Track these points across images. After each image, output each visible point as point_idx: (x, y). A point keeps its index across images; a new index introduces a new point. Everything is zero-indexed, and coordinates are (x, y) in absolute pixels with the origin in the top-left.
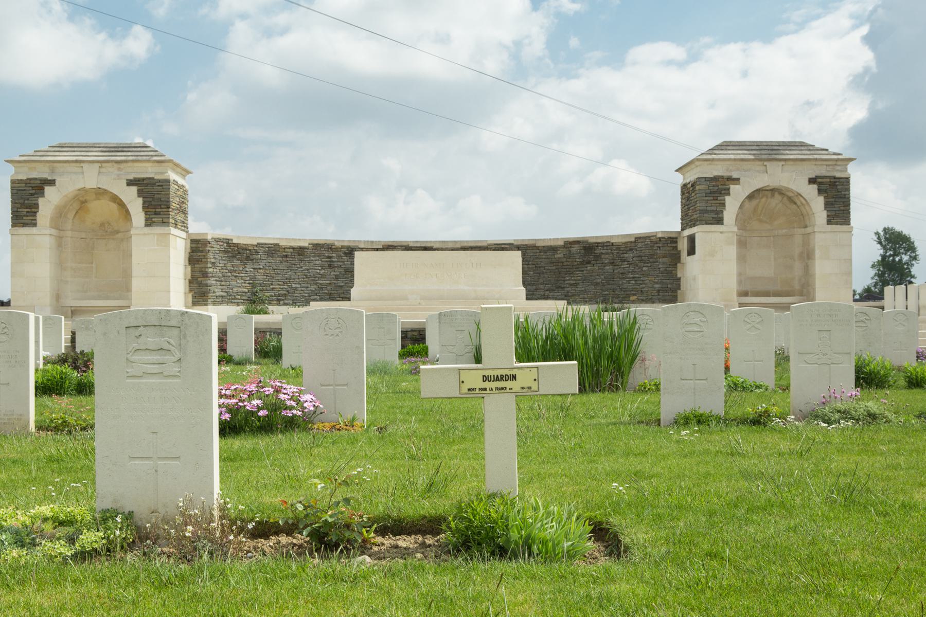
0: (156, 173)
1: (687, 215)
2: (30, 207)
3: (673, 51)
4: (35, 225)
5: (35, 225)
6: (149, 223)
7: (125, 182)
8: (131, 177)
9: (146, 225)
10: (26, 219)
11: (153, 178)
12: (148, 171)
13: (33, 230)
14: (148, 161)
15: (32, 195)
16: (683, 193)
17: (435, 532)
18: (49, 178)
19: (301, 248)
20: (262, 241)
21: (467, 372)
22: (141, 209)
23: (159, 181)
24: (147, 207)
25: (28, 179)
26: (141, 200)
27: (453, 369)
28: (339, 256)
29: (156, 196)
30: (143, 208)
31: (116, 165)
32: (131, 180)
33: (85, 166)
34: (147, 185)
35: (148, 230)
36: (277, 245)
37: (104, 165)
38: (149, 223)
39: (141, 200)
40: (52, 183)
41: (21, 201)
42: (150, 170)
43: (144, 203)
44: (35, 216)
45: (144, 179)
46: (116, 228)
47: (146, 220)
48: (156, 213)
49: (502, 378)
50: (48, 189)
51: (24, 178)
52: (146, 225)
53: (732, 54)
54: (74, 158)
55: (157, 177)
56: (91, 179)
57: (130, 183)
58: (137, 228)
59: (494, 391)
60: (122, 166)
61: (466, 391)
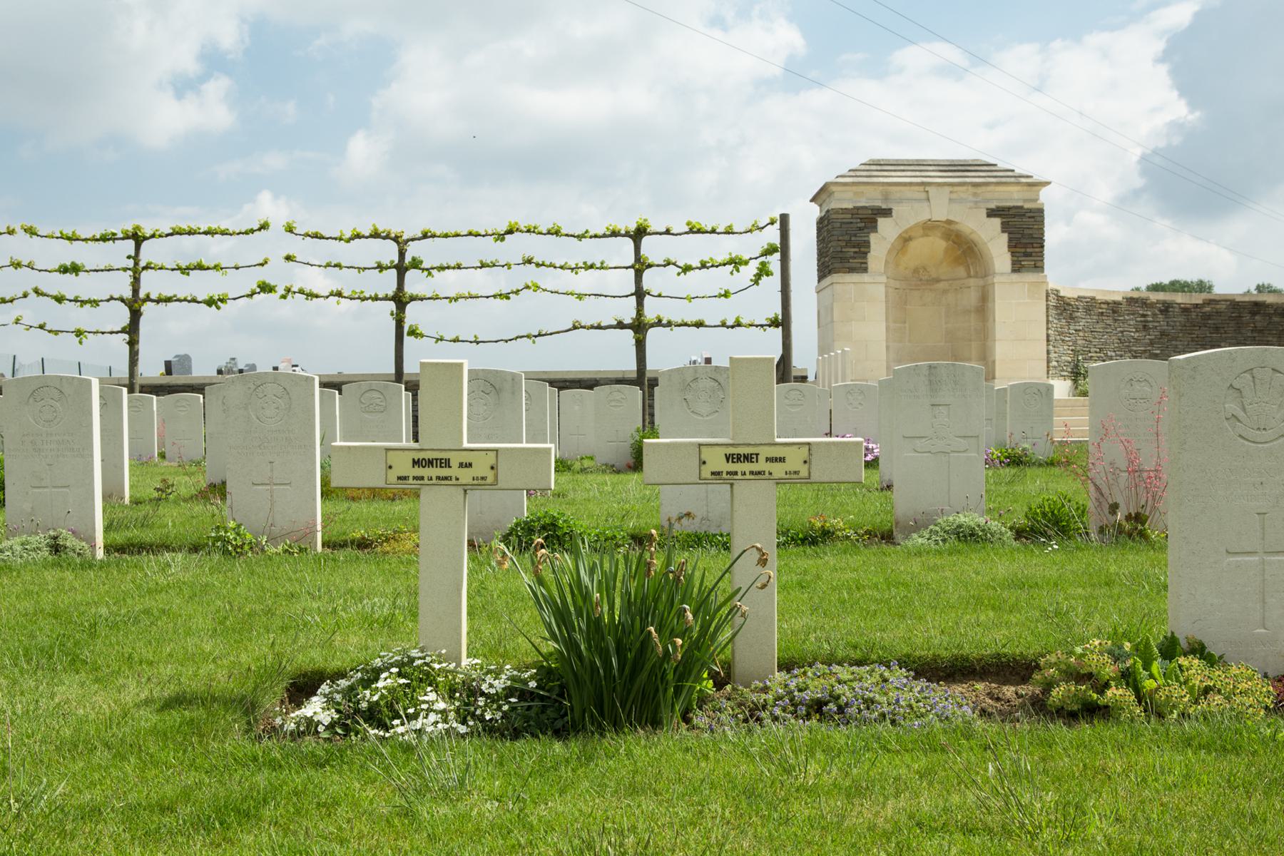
0: (1025, 201)
1: (843, 260)
2: (858, 245)
3: (948, 52)
4: (865, 270)
5: (865, 270)
6: (1017, 268)
7: (985, 212)
8: (992, 206)
9: (1014, 271)
10: (854, 263)
11: (1021, 207)
12: (1013, 197)
13: (864, 277)
14: (1019, 183)
15: (860, 229)
16: (819, 230)
17: (1025, 680)
18: (884, 207)
19: (1115, 302)
20: (1082, 294)
21: (710, 449)
22: (1005, 248)
23: (1030, 210)
24: (1014, 246)
25: (855, 208)
26: (1005, 236)
27: (691, 444)
28: (1154, 315)
29: (1026, 232)
30: (1009, 247)
31: (971, 189)
32: (992, 210)
33: (931, 190)
34: (1014, 216)
35: (1015, 277)
36: (1093, 299)
37: (956, 189)
38: (1017, 268)
39: (1005, 236)
40: (887, 213)
41: (847, 238)
42: (1016, 196)
43: (1010, 240)
44: (865, 258)
45: (1009, 208)
46: (934, 276)
47: (1013, 263)
48: (1027, 255)
49: (739, 459)
50: (882, 222)
51: (850, 206)
52: (1014, 271)
53: (1021, 59)
54: (919, 180)
55: (1027, 206)
56: (940, 210)
57: (992, 213)
58: (1002, 274)
59: (748, 476)
60: (979, 190)
61: (709, 476)
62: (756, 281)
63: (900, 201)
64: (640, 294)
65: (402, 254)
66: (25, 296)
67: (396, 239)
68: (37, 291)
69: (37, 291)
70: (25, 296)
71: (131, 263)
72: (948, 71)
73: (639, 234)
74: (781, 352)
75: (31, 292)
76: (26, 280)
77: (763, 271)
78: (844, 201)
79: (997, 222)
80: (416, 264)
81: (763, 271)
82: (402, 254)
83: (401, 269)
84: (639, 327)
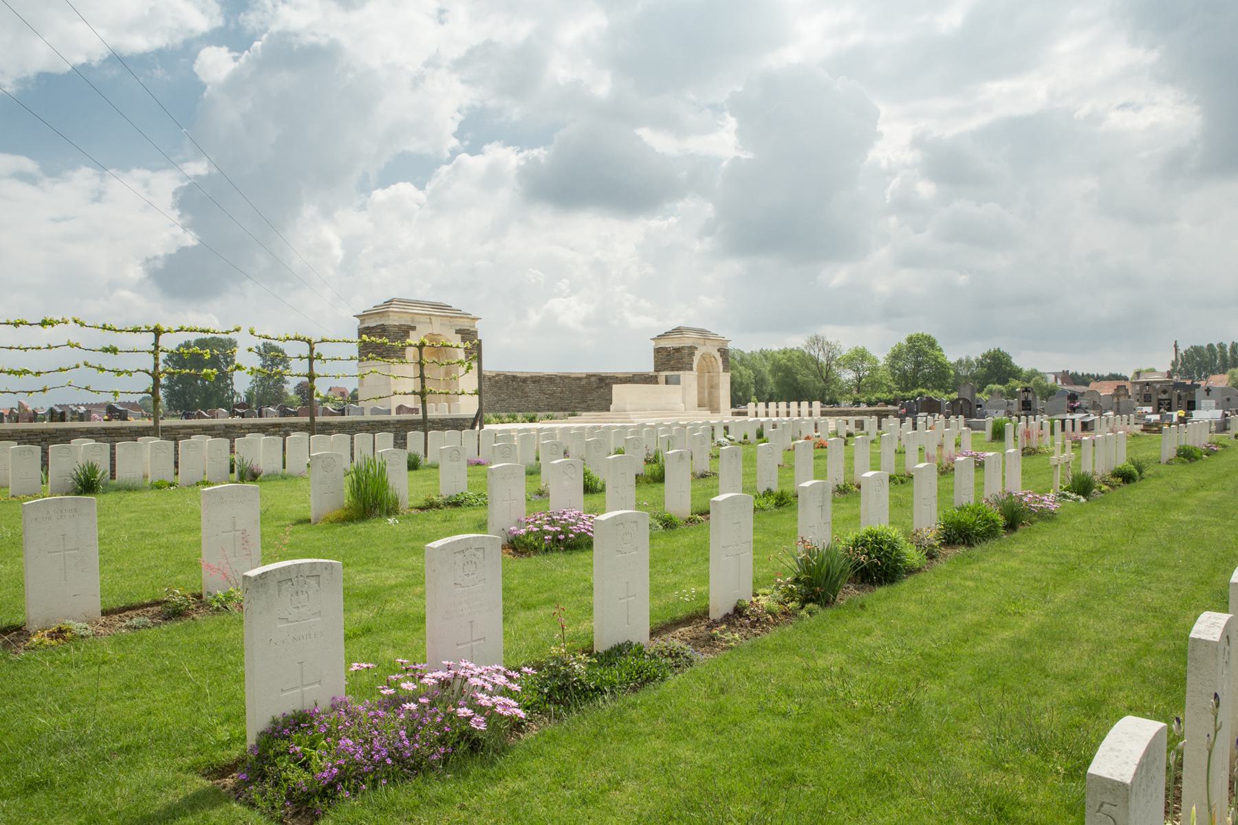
3: (26, 164)
12: (465, 324)
40: (414, 328)
53: (84, 177)
57: (458, 332)
62: (467, 372)
63: (419, 323)
64: (422, 377)
65: (312, 350)
66: (77, 367)
67: (309, 342)
68: (86, 364)
69: (86, 364)
70: (77, 367)
71: (153, 348)
72: (22, 176)
73: (157, 332)
74: (477, 408)
75: (82, 365)
76: (77, 356)
77: (469, 368)
78: (668, 344)
79: (459, 336)
80: (319, 357)
81: (469, 368)
82: (312, 350)
83: (311, 360)
84: (422, 394)
